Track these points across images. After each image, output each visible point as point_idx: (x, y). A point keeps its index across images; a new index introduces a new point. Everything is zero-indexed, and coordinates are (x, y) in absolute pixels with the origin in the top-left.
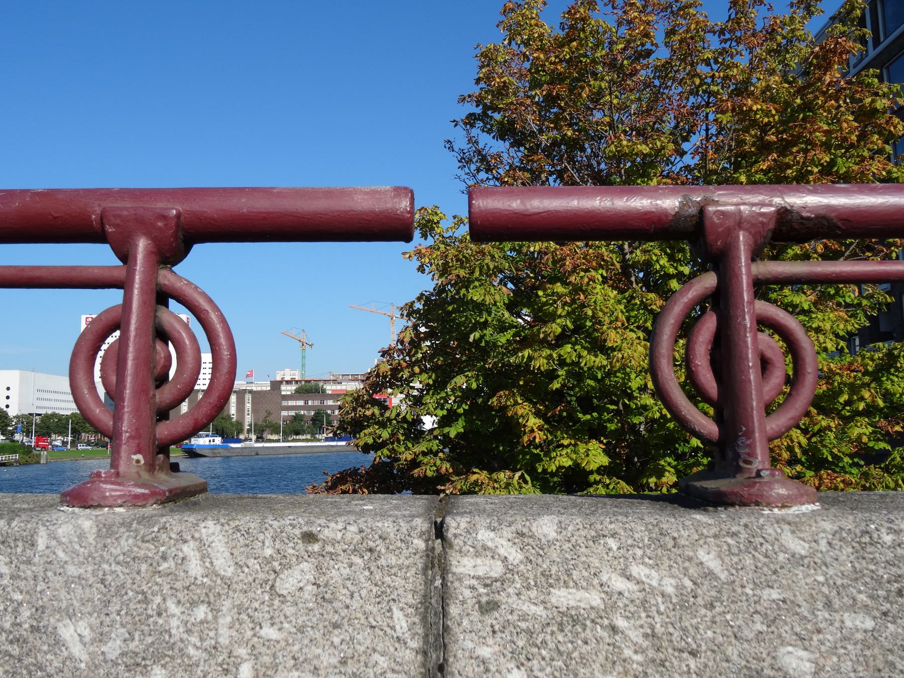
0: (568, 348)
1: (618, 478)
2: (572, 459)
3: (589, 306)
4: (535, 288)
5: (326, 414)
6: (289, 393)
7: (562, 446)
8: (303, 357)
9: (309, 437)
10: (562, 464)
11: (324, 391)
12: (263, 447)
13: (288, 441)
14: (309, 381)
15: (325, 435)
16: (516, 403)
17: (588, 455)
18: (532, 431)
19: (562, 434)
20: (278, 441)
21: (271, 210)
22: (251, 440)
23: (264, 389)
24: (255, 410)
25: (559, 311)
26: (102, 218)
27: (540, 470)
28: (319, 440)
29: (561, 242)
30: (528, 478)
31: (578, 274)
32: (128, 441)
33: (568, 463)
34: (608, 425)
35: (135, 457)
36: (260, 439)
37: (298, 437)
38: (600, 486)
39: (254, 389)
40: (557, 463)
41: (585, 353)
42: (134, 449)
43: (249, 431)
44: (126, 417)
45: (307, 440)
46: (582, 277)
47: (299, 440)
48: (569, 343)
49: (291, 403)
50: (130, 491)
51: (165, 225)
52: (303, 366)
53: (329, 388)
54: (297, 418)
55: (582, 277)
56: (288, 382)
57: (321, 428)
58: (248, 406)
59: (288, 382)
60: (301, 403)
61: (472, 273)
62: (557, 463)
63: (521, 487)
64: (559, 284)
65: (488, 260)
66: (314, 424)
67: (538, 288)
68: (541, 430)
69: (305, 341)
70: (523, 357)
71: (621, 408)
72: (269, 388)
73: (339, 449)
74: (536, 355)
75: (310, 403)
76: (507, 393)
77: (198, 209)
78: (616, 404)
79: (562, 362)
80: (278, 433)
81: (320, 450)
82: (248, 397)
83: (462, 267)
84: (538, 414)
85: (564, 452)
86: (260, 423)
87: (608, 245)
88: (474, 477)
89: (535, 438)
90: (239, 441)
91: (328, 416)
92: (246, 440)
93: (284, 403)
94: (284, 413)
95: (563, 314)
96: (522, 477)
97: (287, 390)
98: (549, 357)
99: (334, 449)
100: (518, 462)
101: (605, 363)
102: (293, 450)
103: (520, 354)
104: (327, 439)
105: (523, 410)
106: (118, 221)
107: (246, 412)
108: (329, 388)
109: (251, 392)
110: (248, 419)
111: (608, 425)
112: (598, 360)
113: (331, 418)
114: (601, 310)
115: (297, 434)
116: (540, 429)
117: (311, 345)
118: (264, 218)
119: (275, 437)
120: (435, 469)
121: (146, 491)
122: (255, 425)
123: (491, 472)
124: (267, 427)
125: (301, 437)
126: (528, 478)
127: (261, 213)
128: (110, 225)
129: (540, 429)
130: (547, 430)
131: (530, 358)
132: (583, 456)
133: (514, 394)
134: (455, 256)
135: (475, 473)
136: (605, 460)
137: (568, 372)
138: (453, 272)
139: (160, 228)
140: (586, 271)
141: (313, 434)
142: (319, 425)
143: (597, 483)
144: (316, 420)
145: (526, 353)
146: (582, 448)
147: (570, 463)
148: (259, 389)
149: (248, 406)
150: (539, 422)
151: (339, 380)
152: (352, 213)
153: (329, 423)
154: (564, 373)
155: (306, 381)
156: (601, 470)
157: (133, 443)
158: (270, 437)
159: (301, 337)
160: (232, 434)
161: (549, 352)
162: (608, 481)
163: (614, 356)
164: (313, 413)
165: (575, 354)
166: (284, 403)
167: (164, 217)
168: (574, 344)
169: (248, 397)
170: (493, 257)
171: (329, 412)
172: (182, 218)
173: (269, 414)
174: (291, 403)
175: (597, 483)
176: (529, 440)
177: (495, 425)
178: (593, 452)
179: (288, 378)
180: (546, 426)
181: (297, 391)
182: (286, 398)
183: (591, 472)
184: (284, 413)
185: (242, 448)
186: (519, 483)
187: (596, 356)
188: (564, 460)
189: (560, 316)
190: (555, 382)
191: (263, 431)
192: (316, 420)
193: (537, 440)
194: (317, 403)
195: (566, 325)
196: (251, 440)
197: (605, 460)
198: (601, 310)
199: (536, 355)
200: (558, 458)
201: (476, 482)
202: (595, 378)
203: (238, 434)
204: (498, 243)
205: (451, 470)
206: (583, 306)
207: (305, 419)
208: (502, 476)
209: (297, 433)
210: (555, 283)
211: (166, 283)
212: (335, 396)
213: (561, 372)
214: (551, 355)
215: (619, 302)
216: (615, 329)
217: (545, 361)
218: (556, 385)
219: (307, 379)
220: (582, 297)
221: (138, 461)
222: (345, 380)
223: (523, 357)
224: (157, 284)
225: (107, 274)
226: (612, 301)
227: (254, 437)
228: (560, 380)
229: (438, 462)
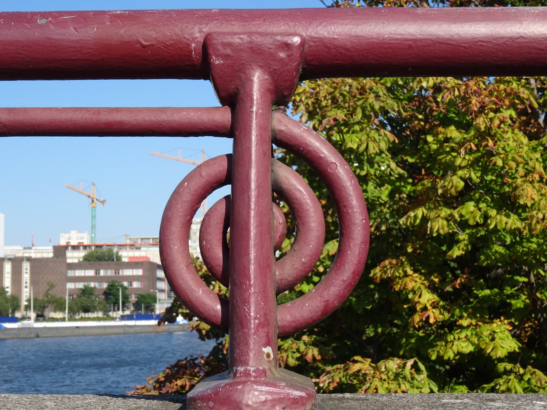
0: (471, 206)
1: (534, 367)
2: (473, 344)
3: (499, 154)
4: (424, 132)
5: (122, 286)
6: (76, 261)
7: (461, 327)
8: (94, 217)
9: (100, 314)
10: (461, 350)
11: (119, 258)
12: (45, 328)
13: (75, 320)
14: (101, 246)
15: (120, 313)
16: (406, 275)
17: (493, 339)
18: (425, 309)
19: (461, 312)
20: (63, 320)
21: (419, 36)
22: (29, 318)
23: (45, 255)
24: (34, 282)
25: (458, 162)
26: (205, 46)
27: (434, 357)
28: (113, 319)
29: (457, 75)
30: (422, 366)
31: (487, 114)
32: (257, 330)
33: (467, 348)
34: (513, 302)
35: (264, 350)
36: (40, 317)
37: (87, 315)
38: (512, 377)
39: (33, 256)
40: (455, 348)
41: (493, 213)
42: (264, 340)
43: (27, 308)
44: (252, 300)
45: (98, 319)
46: (491, 120)
47: (89, 319)
48: (471, 200)
49: (79, 273)
50: (288, 394)
51: (289, 56)
52: (93, 227)
53: (126, 255)
54: (86, 292)
55: (491, 120)
56: (75, 248)
57: (116, 303)
58: (26, 277)
59: (75, 248)
60: (91, 273)
61: (352, 113)
62: (455, 348)
63: (413, 378)
64: (453, 128)
65: (371, 98)
66: (107, 299)
67: (426, 132)
68: (434, 307)
69: (96, 196)
70: (415, 217)
71: (533, 279)
72: (51, 255)
73: (138, 329)
74: (432, 215)
75: (102, 273)
76: (394, 262)
77: (326, 34)
78: (527, 275)
79: (463, 224)
80: (62, 309)
81: (115, 331)
82: (26, 266)
83: (339, 107)
84: (433, 288)
85: (463, 335)
86: (41, 297)
87: (519, 80)
88: (356, 367)
89: (428, 318)
90: (15, 320)
91: (124, 288)
92: (23, 318)
93: (70, 273)
94: (70, 286)
95: (464, 164)
96: (415, 366)
97: (73, 257)
98: (449, 219)
99: (131, 330)
100: (400, 347)
101: (519, 224)
102: (81, 331)
103: (412, 214)
104: (123, 318)
105: (414, 284)
106: (228, 51)
107: (24, 285)
108: (126, 255)
109: (29, 259)
110: (26, 293)
111: (513, 302)
112: (510, 221)
113: (128, 292)
114: (514, 159)
115: (86, 310)
116: (435, 306)
117: (103, 202)
118: (410, 46)
119: (59, 315)
120: (298, 355)
121: (303, 394)
122: (35, 300)
123: (375, 361)
124: (49, 302)
125: (90, 315)
126: (422, 366)
127: (407, 40)
128: (217, 56)
129: (435, 306)
130: (443, 307)
131: (425, 220)
132: (488, 340)
133: (402, 263)
134: (330, 94)
135: (357, 362)
136: (512, 345)
137: (471, 236)
138: (329, 114)
139: (282, 60)
140: (496, 111)
141: (106, 311)
142: (114, 300)
143: (507, 372)
144: (110, 294)
145: (420, 212)
146: (486, 330)
147: (471, 348)
148: (39, 256)
149: (26, 277)
150: (434, 297)
151: (137, 245)
152: (522, 40)
153: (126, 298)
154: (466, 237)
155: (97, 246)
156: (511, 357)
157: (262, 332)
158: (53, 315)
159: (91, 191)
160: (7, 311)
161: (449, 211)
162: (522, 371)
163: (532, 217)
164: (105, 285)
165: (479, 214)
166: (70, 273)
167: (287, 46)
168: (477, 202)
169: (26, 266)
170: (377, 97)
171: (125, 284)
172: (306, 47)
173: (52, 286)
174: (79, 273)
175: (507, 372)
176: (421, 320)
177: (373, 301)
178: (500, 334)
179: (74, 242)
180: (441, 303)
181: (86, 259)
182: (72, 266)
183: (501, 360)
184: (70, 286)
185: (18, 329)
186: (411, 373)
187: (508, 216)
188: (464, 344)
189: (461, 168)
190: (455, 248)
191: (44, 307)
192: (110, 294)
193: (432, 321)
194: (110, 273)
195: (470, 179)
196: (29, 318)
197: (512, 345)
198: (514, 159)
199: (432, 215)
200: (456, 343)
201: (356, 374)
202: (503, 244)
203: (13, 311)
204: (378, 78)
205: (319, 357)
206: (491, 154)
207: (96, 293)
208: (393, 364)
209: (86, 310)
210: (448, 126)
211: (283, 128)
212: (134, 264)
213: (463, 236)
214: (451, 215)
215: (534, 150)
216: (532, 182)
217: (445, 223)
218: (457, 252)
219: (98, 243)
220: (491, 143)
221: (268, 355)
222: (145, 245)
223: (415, 217)
224: (273, 131)
225: (194, 118)
226: (526, 148)
227: (33, 315)
228: (462, 245)
229: (302, 348)
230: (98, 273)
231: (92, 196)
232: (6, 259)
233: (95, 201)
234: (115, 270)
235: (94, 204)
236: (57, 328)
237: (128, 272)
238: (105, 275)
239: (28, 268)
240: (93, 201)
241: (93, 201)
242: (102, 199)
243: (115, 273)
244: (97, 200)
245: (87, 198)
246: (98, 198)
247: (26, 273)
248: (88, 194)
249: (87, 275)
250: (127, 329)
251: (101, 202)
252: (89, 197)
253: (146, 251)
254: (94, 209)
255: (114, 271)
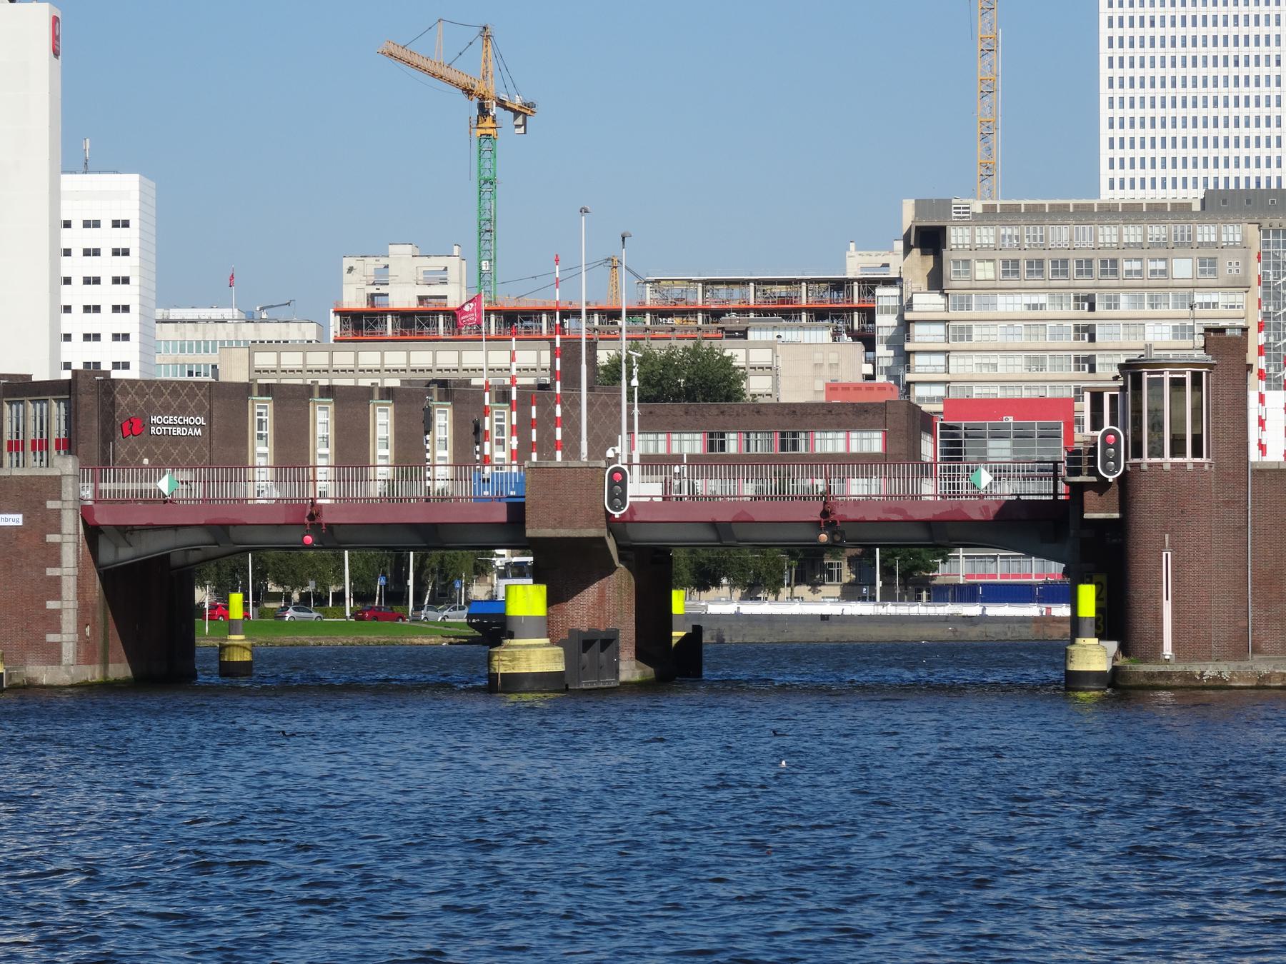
8: (488, 183)
52: (486, 229)
69: (493, 88)
75: (733, 444)
117: (521, 113)
159: (468, 71)
230: (717, 445)
231: (480, 88)
232: (255, 391)
233: (494, 110)
234: (711, 435)
235: (489, 123)
236: (770, 619)
237: (831, 442)
238: (744, 452)
239: (268, 417)
240: (483, 111)
241: (483, 111)
242: (518, 101)
243: (783, 448)
244: (501, 104)
245: (463, 97)
246: (503, 97)
247: (260, 436)
248: (464, 80)
249: (854, 448)
250: (962, 628)
251: (517, 113)
252: (469, 92)
253: (770, 346)
254: (486, 145)
255: (776, 438)
